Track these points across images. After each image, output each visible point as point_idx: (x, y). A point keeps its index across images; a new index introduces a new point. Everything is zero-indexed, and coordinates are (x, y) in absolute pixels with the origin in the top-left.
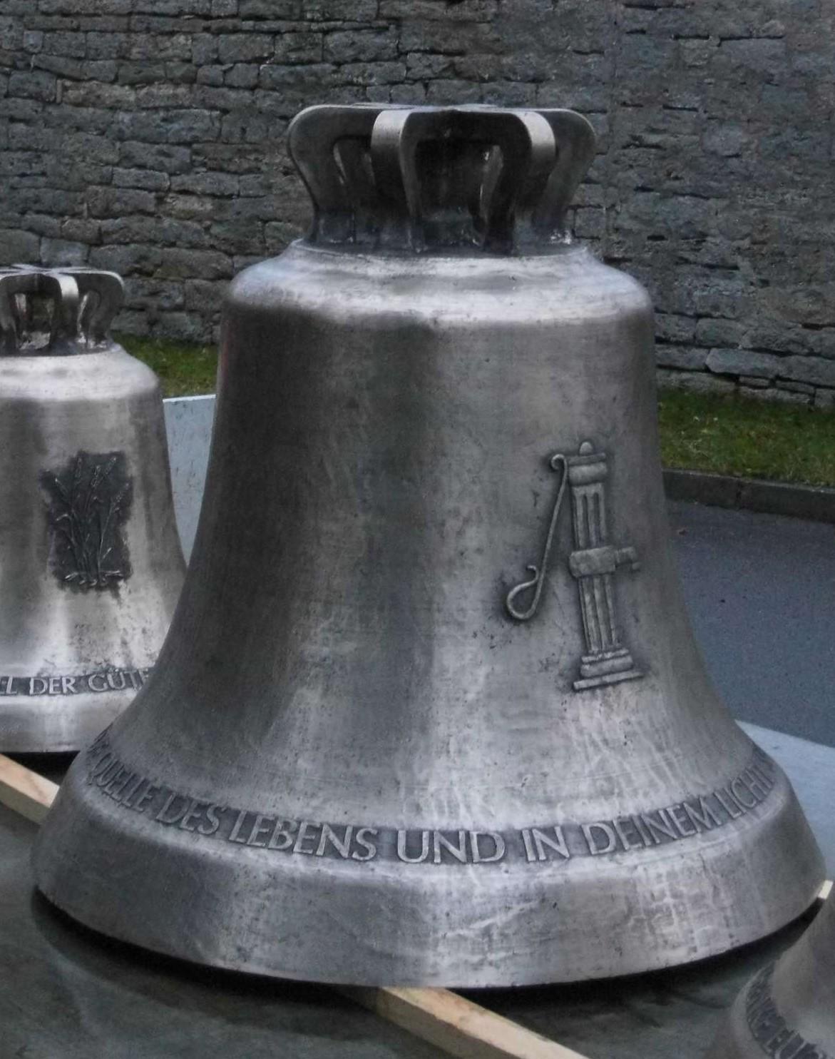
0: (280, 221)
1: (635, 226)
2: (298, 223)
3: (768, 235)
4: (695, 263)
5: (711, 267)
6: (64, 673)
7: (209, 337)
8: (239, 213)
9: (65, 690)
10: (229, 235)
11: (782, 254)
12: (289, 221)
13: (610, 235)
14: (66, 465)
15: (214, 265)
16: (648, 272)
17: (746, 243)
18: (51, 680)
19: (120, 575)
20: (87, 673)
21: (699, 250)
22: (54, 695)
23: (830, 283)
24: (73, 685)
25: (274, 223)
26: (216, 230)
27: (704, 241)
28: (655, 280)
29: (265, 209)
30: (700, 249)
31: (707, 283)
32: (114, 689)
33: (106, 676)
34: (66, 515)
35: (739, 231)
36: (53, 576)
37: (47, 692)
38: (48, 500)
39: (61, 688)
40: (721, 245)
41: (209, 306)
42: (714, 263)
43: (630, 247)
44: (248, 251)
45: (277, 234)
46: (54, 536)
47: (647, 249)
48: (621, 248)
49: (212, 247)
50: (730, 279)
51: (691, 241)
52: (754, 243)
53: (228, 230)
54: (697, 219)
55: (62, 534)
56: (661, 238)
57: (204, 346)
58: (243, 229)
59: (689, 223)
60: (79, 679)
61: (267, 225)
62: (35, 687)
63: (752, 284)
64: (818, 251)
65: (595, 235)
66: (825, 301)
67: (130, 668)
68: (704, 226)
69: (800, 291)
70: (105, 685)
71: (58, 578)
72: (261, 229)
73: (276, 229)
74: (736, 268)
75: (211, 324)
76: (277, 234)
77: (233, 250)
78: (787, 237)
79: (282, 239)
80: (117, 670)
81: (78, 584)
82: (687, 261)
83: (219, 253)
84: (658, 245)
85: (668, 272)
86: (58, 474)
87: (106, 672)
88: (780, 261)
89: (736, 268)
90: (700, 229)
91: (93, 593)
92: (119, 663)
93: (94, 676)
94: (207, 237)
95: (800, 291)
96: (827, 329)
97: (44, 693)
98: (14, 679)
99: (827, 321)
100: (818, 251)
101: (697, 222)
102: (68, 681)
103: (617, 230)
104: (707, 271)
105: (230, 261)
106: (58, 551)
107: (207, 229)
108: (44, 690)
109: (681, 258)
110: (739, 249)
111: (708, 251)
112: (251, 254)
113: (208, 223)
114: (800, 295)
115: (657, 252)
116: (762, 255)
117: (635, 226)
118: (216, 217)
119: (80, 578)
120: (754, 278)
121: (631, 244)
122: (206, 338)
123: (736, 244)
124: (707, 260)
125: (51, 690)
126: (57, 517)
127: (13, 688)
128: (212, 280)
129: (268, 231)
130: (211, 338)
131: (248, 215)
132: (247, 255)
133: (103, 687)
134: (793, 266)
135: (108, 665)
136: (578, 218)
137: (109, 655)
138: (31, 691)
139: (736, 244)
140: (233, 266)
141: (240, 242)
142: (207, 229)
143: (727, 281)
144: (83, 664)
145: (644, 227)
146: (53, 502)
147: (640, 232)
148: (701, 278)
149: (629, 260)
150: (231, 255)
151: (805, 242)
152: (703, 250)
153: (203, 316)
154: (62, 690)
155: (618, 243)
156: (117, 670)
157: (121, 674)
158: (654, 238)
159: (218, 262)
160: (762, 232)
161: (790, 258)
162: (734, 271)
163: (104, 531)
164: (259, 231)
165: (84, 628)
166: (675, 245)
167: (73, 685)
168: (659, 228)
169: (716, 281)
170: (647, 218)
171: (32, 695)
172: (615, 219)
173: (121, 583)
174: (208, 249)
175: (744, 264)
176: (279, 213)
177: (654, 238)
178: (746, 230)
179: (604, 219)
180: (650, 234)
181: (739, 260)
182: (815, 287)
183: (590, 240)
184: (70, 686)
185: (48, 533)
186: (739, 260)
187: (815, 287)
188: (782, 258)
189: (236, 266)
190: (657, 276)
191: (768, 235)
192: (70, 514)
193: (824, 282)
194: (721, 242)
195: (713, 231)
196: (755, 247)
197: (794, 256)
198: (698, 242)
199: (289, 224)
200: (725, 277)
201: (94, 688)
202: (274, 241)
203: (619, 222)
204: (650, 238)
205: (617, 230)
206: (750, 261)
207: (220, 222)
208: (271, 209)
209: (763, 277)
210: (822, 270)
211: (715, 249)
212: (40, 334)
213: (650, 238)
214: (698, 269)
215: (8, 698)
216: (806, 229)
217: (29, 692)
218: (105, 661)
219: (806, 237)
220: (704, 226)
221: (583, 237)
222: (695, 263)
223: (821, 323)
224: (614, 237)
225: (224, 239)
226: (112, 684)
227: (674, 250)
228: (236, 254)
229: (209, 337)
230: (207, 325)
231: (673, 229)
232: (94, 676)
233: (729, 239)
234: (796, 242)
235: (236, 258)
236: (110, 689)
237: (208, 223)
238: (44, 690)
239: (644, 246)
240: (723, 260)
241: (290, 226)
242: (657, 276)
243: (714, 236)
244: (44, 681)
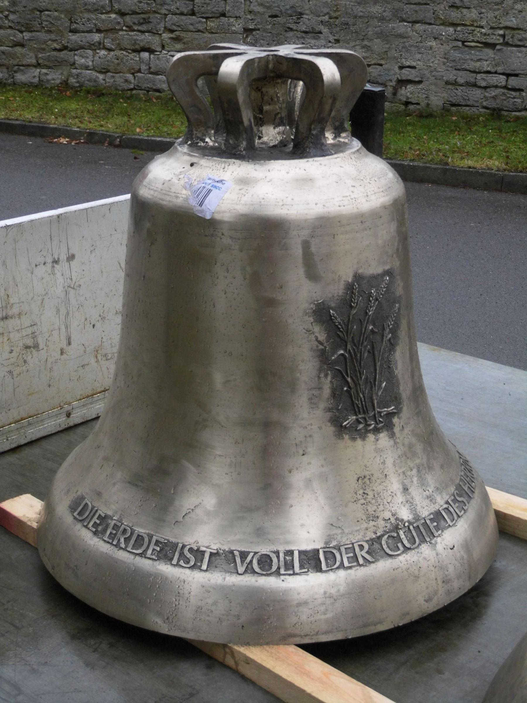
0: (50, 11)
1: (261, 9)
2: (61, 12)
3: (339, 13)
4: (296, 30)
5: (306, 32)
6: (356, 538)
7: (12, 80)
8: (25, 7)
9: (361, 561)
10: (19, 20)
11: (347, 24)
12: (56, 11)
13: (246, 15)
14: (341, 292)
15: (12, 38)
16: (269, 37)
17: (327, 18)
18: (343, 549)
19: (395, 411)
20: (379, 534)
21: (298, 23)
22: (350, 568)
23: (375, 40)
24: (368, 552)
25: (47, 13)
26: (12, 17)
27: (302, 18)
28: (274, 41)
29: (41, 4)
30: (300, 22)
31: (303, 42)
32: (409, 549)
33: (398, 533)
34: (342, 352)
35: (322, 12)
36: (329, 424)
37: (342, 566)
38: (322, 337)
39: (355, 558)
40: (312, 19)
41: (11, 62)
42: (308, 30)
43: (258, 22)
44: (32, 29)
45: (48, 19)
46: (329, 378)
47: (268, 23)
48: (253, 22)
49: (10, 27)
50: (317, 39)
51: (294, 18)
52: (330, 18)
53: (20, 17)
54: (297, 5)
55: (340, 375)
56: (276, 16)
57: (9, 85)
58: (29, 16)
59: (292, 7)
60: (371, 542)
61: (43, 13)
62: (326, 559)
63: (330, 42)
64: (368, 22)
65: (238, 16)
66: (372, 51)
67: (417, 518)
68: (301, 9)
69: (357, 45)
70: (400, 545)
71: (335, 426)
72: (39, 16)
73: (48, 16)
74: (320, 33)
75: (13, 72)
76: (48, 19)
77: (23, 29)
78: (350, 14)
79: (52, 22)
80: (407, 524)
81: (356, 430)
82: (291, 29)
83: (15, 31)
84: (275, 21)
85: (281, 36)
86: (333, 305)
87: (396, 528)
88: (346, 28)
89: (320, 33)
90: (299, 11)
91: (371, 437)
92: (405, 514)
93: (386, 537)
94: (6, 22)
95: (357, 45)
96: (407, 69)
97: (338, 568)
98: (300, 552)
99: (373, 62)
100: (368, 22)
101: (297, 6)
102: (361, 547)
103: (250, 12)
104: (304, 35)
105: (21, 35)
106: (334, 394)
107: (6, 17)
108: (338, 564)
109: (289, 28)
110: (322, 22)
111: (304, 23)
112: (34, 31)
113: (7, 13)
114: (358, 47)
115: (274, 24)
116: (336, 25)
117: (261, 9)
118: (11, 10)
119: (358, 422)
120: (331, 38)
121: (259, 20)
122: (10, 81)
123: (320, 19)
124: (304, 29)
125: (346, 564)
126: (333, 355)
127: (302, 567)
128: (12, 47)
129: (44, 18)
130: (14, 81)
131: (31, 8)
132: (31, 31)
133: (399, 549)
134: (354, 31)
135: (397, 519)
136: (227, 6)
137: (394, 508)
138: (324, 567)
139: (320, 19)
140: (23, 38)
141: (27, 24)
142: (6, 17)
143: (316, 41)
144: (372, 523)
145: (265, 10)
146: (329, 337)
147: (264, 13)
148: (300, 39)
149: (259, 30)
150: (21, 32)
151: (361, 17)
152: (301, 23)
153: (8, 69)
154: (357, 561)
155: (252, 20)
156: (407, 524)
157: (411, 527)
158: (272, 16)
159: (14, 36)
160: (335, 11)
161: (352, 26)
162: (319, 35)
163: (378, 364)
164: (38, 18)
165: (366, 480)
166: (285, 20)
167: (368, 552)
168: (275, 11)
169: (309, 41)
170: (268, 5)
171: (326, 571)
172: (250, 6)
173: (395, 420)
174: (7, 28)
175: (325, 30)
176: (49, 7)
177: (272, 16)
178: (325, 10)
179: (243, 6)
180: (270, 14)
181: (321, 28)
182: (366, 43)
183: (235, 19)
184: (363, 553)
185: (322, 375)
186: (321, 28)
187: (366, 43)
188: (348, 27)
189: (25, 38)
190: (275, 39)
191: (339, 13)
192: (345, 350)
193: (371, 40)
194: (311, 18)
195: (307, 12)
196: (331, 20)
197: (354, 25)
198: (298, 18)
199: (56, 13)
200: (314, 38)
201: (390, 553)
202: (47, 23)
203: (252, 7)
204: (270, 17)
205: (250, 12)
206: (329, 29)
207: (14, 13)
208: (44, 4)
209: (336, 38)
210: (370, 33)
211: (307, 22)
212: (271, 128)
213: (270, 17)
214: (299, 34)
215: (298, 577)
216: (360, 9)
217: (321, 568)
218: (393, 515)
219: (361, 14)
220: (301, 9)
221: (231, 17)
222: (296, 30)
223: (370, 63)
224: (249, 17)
225: (17, 23)
226: (408, 545)
227: (284, 23)
228: (24, 31)
229: (12, 80)
230: (10, 73)
231: (283, 10)
232: (386, 537)
233: (317, 16)
234: (356, 17)
235: (25, 34)
236: (407, 549)
237: (7, 13)
238: (338, 564)
239: (267, 21)
240: (312, 28)
241: (56, 14)
242: (275, 39)
243: (307, 15)
244: (335, 551)
